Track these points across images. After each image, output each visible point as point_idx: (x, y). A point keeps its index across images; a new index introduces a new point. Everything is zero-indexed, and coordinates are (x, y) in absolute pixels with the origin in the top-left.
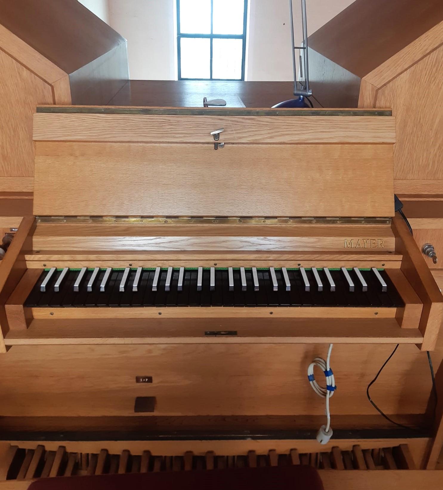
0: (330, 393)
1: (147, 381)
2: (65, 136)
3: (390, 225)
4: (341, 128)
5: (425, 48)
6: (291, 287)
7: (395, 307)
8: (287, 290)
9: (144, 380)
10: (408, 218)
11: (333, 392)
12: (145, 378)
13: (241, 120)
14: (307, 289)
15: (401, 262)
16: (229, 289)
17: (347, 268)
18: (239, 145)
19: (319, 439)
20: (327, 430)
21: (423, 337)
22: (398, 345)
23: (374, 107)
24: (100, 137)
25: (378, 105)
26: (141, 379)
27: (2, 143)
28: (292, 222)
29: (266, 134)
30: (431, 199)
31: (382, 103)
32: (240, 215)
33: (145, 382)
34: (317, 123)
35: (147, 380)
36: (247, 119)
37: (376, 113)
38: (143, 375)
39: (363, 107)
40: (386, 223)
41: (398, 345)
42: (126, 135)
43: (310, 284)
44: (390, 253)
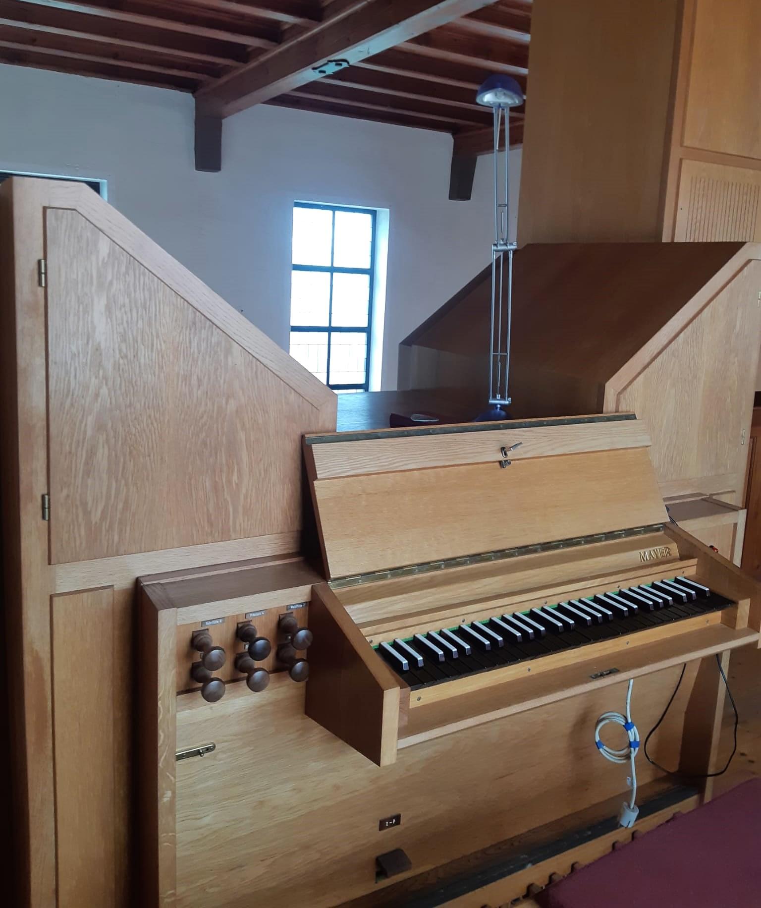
0: (634, 749)
1: (395, 822)
2: (353, 470)
3: (663, 532)
4: (606, 434)
5: (652, 353)
6: (424, 662)
7: (718, 609)
8: (419, 666)
9: (391, 823)
10: (678, 521)
11: (637, 749)
12: (391, 819)
13: (520, 433)
14: (442, 659)
15: (696, 566)
16: (485, 648)
17: (450, 627)
18: (360, 477)
19: (624, 823)
20: (632, 807)
21: (759, 632)
22: (685, 665)
23: (617, 411)
24: (391, 466)
25: (620, 410)
26: (387, 823)
27: (247, 490)
28: (361, 582)
29: (467, 450)
30: (677, 501)
31: (624, 408)
32: (420, 561)
33: (391, 825)
34: (586, 431)
35: (394, 821)
36: (526, 431)
37: (624, 417)
38: (389, 815)
39: (607, 413)
40: (387, 577)
41: (685, 665)
42: (417, 461)
43: (543, 626)
44: (674, 560)
